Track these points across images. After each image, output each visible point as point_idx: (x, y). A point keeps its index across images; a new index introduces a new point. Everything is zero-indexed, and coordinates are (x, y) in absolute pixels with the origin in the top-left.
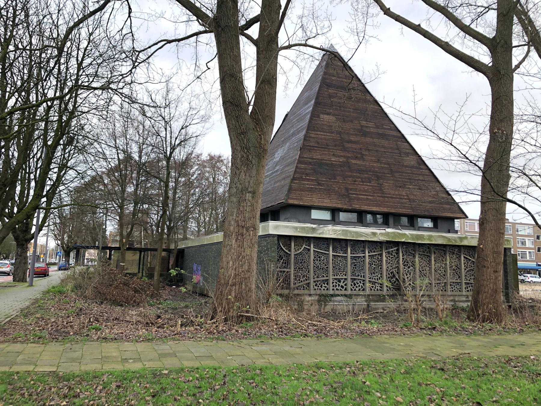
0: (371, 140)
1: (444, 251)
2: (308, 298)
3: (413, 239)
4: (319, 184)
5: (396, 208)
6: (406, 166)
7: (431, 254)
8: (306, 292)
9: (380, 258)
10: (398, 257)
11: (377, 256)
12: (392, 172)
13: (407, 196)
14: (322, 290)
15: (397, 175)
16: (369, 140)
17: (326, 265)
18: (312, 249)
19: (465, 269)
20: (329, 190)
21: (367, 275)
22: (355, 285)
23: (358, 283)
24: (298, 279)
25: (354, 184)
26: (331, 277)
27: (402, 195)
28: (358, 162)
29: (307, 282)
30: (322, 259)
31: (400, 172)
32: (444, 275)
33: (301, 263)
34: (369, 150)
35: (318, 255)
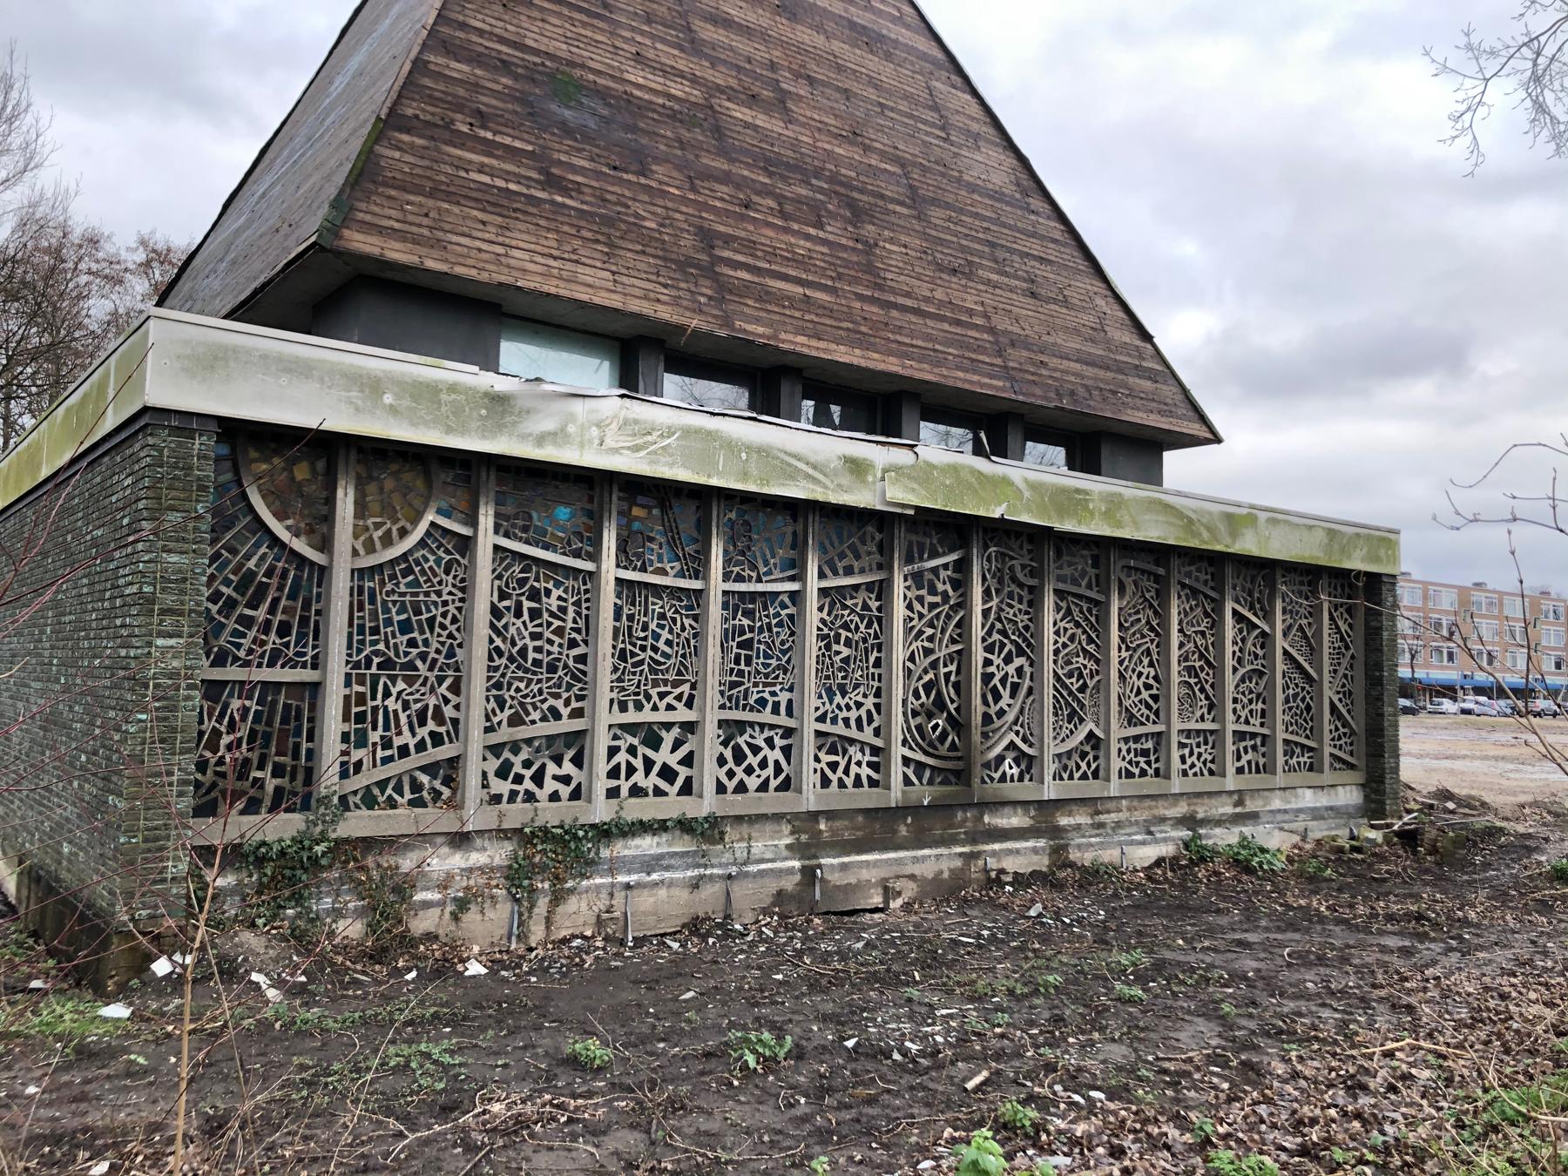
0: (820, 40)
1: (1157, 579)
2: (445, 861)
3: (1042, 509)
4: (552, 182)
5: (938, 364)
6: (972, 188)
7: (1107, 592)
8: (433, 818)
9: (874, 604)
10: (964, 604)
11: (861, 596)
12: (915, 199)
13: (986, 316)
14: (544, 804)
15: (937, 215)
16: (805, 35)
17: (573, 644)
18: (487, 537)
19: (1235, 670)
20: (609, 221)
21: (812, 702)
22: (739, 757)
23: (756, 750)
24: (374, 737)
25: (743, 217)
26: (604, 718)
27: (961, 309)
28: (761, 120)
29: (446, 751)
30: (554, 603)
31: (947, 206)
32: (1155, 698)
33: (405, 627)
34: (811, 81)
35: (521, 581)
